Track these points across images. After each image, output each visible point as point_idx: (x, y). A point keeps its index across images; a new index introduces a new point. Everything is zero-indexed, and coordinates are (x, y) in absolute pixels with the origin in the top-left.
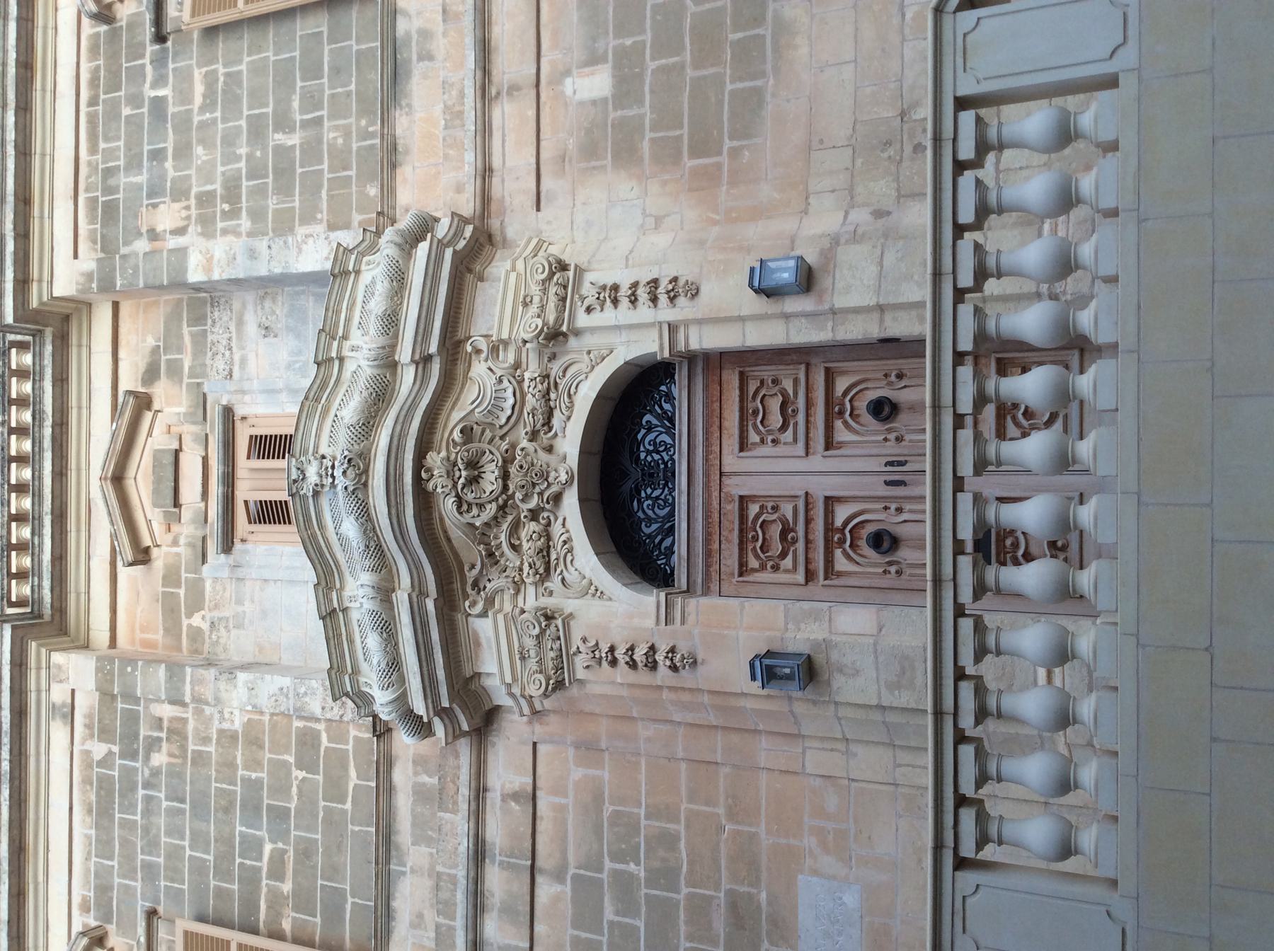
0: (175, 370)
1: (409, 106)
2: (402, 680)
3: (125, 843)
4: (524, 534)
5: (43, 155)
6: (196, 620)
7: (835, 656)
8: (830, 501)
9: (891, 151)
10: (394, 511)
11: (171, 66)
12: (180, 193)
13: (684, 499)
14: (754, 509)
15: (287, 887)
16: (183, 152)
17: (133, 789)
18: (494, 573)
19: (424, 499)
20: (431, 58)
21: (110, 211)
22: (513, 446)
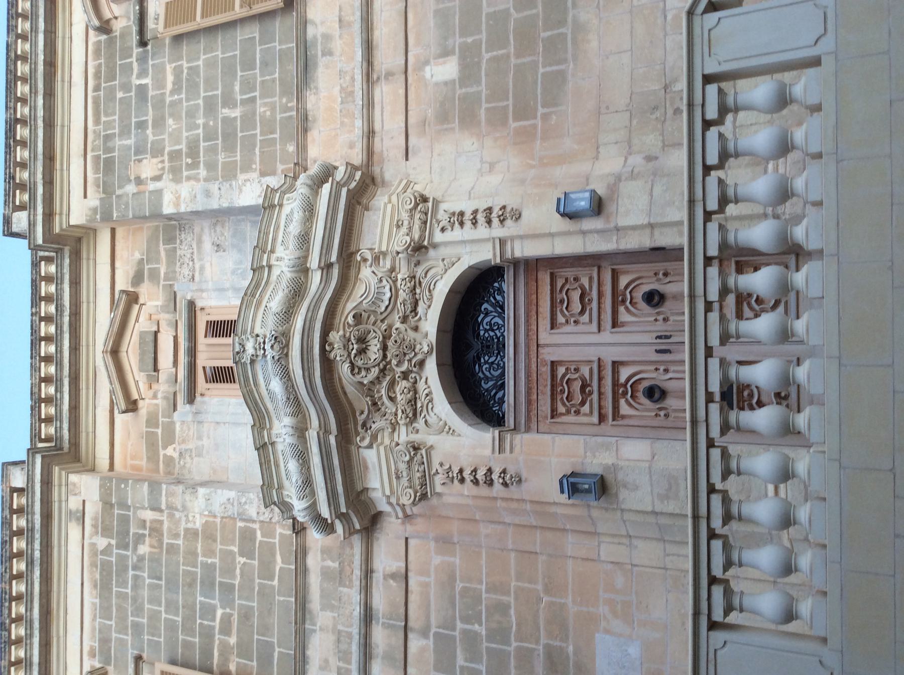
0: (154, 276)
1: (316, 88)
2: (313, 493)
3: (119, 608)
4: (398, 389)
5: (63, 126)
6: (170, 451)
7: (620, 476)
8: (616, 365)
9: (657, 114)
10: (306, 374)
11: (150, 62)
12: (157, 151)
13: (512, 363)
14: (561, 370)
15: (233, 640)
16: (159, 123)
17: (125, 569)
18: (377, 416)
19: (328, 365)
20: (330, 53)
21: (109, 165)
22: (390, 327)
